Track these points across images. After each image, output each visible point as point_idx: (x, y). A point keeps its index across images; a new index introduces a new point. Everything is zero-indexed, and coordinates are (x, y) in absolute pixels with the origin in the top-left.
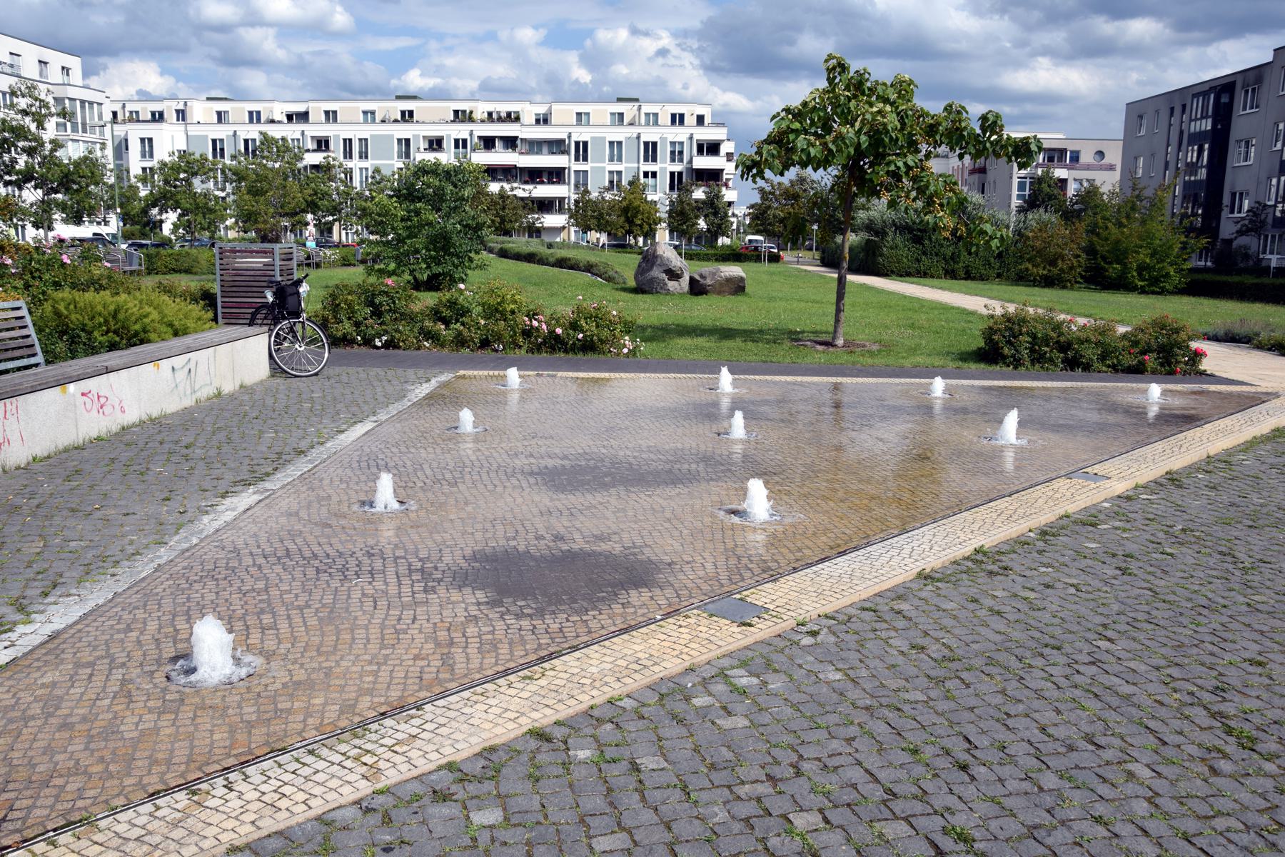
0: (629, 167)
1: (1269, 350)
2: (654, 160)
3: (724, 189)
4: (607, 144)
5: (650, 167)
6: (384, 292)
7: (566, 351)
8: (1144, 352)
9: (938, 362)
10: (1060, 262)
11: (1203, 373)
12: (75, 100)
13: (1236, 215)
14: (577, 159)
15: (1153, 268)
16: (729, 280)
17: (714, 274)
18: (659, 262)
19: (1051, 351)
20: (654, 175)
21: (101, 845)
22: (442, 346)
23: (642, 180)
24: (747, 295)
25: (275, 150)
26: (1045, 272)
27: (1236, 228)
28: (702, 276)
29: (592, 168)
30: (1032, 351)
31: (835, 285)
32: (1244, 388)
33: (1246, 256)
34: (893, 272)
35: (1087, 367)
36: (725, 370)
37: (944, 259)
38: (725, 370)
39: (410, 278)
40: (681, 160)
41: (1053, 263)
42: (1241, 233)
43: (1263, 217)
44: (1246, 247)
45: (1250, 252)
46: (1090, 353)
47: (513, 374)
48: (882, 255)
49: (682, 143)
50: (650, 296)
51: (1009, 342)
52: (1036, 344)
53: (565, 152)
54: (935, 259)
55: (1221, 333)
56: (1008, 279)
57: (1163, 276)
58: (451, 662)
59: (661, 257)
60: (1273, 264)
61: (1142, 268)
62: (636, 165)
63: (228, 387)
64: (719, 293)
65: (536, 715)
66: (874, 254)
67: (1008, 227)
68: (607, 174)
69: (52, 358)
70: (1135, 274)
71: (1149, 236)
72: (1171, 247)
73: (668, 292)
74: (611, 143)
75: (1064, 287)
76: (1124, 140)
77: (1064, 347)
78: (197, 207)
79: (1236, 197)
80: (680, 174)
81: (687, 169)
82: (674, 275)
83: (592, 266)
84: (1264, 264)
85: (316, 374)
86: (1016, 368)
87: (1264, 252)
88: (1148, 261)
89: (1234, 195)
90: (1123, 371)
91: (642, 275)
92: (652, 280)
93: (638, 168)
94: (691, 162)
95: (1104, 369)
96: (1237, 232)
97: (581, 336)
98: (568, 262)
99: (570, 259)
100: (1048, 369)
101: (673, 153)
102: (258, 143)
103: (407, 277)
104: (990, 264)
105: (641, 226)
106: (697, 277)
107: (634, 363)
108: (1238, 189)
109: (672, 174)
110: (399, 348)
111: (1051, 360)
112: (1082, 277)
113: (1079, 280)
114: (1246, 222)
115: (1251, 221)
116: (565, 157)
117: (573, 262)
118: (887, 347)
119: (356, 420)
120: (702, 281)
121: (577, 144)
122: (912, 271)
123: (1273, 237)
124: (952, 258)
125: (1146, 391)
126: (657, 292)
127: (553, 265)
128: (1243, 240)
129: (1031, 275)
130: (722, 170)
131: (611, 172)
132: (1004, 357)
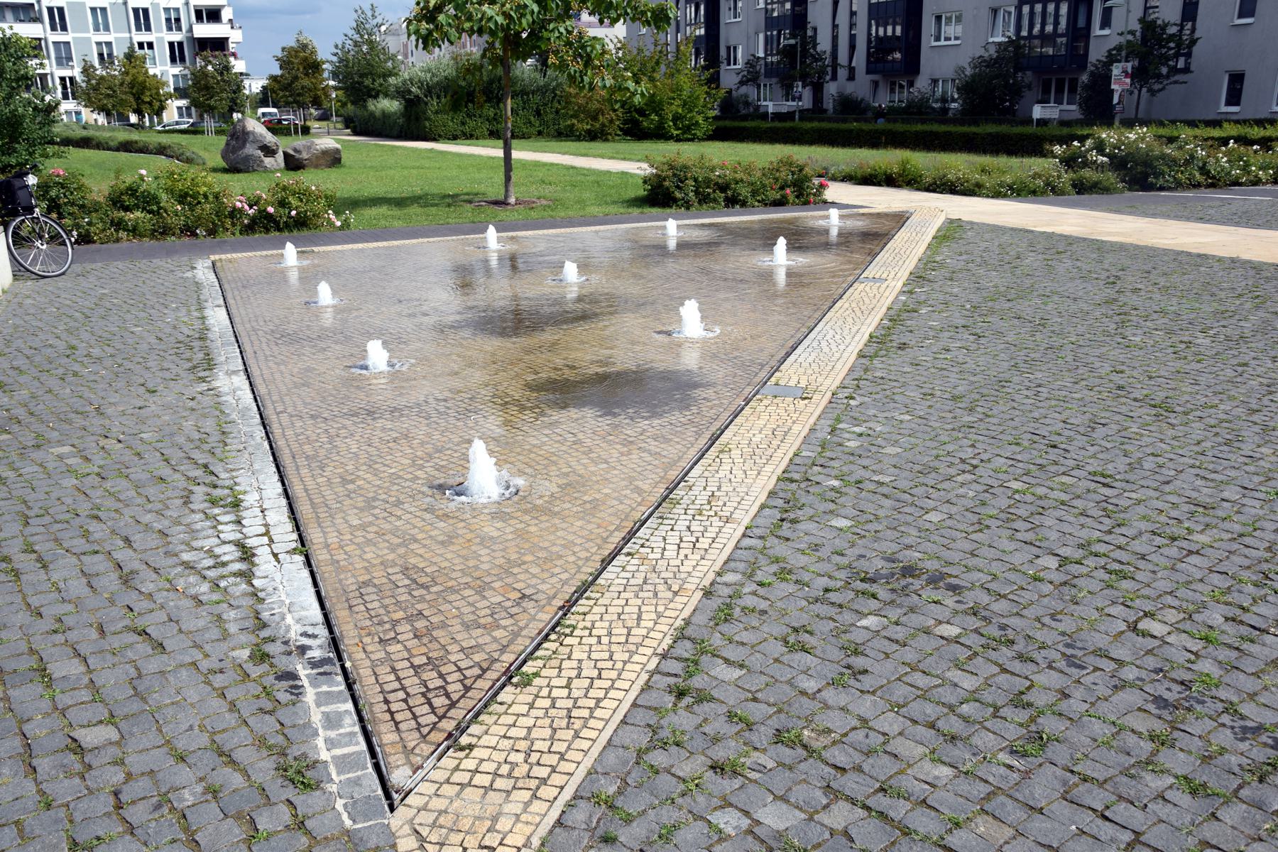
0: (120, 37)
1: (842, 181)
2: (148, 28)
3: (232, 59)
4: (89, 11)
5: (144, 37)
7: (279, 230)
8: (782, 188)
9: (613, 209)
10: (601, 117)
11: (825, 202)
13: (732, 67)
14: (53, 28)
15: (685, 117)
16: (325, 153)
17: (309, 148)
18: (251, 138)
19: (714, 191)
20: (150, 46)
21: (514, 589)
22: (142, 236)
23: (139, 52)
26: (589, 127)
27: (737, 79)
28: (295, 150)
29: (116, 39)
30: (697, 193)
33: (747, 104)
34: (440, 136)
35: (744, 204)
36: (491, 229)
37: (488, 120)
38: (491, 229)
40: (179, 29)
41: (595, 118)
42: (742, 83)
43: (758, 68)
44: (746, 96)
45: (750, 100)
46: (744, 192)
47: (290, 250)
48: (428, 119)
49: (177, 10)
50: (246, 175)
51: (678, 187)
52: (700, 187)
53: (37, 19)
54: (480, 120)
56: (548, 135)
57: (693, 124)
59: (253, 133)
60: (770, 110)
61: (676, 118)
62: (127, 35)
64: (316, 167)
66: (417, 119)
67: (168, 86)
68: (94, 46)
69: (727, 206)
70: (671, 124)
71: (678, 89)
72: (697, 98)
73: (266, 170)
74: (93, 10)
75: (606, 140)
77: (723, 188)
79: (731, 50)
80: (180, 44)
81: (188, 38)
82: (269, 151)
83: (165, 148)
84: (762, 110)
85: (63, 274)
86: (688, 208)
87: (759, 100)
88: (680, 111)
89: (728, 48)
90: (771, 205)
91: (233, 153)
92: (247, 158)
93: (131, 38)
94: (190, 30)
95: (756, 204)
96: (740, 83)
97: (293, 213)
98: (135, 146)
99: (136, 142)
100: (714, 208)
101: (168, 20)
104: (530, 123)
105: (150, 103)
106: (292, 152)
107: (345, 233)
108: (732, 43)
109: (171, 44)
110: (94, 242)
111: (715, 200)
112: (621, 129)
113: (619, 132)
114: (745, 73)
115: (748, 72)
116: (39, 26)
117: (141, 145)
118: (556, 203)
120: (297, 156)
121: (50, 10)
122: (459, 133)
123: (765, 85)
124: (495, 119)
125: (827, 217)
126: (254, 170)
127: (117, 150)
128: (744, 90)
129: (577, 130)
130: (227, 39)
131: (99, 44)
132: (675, 200)
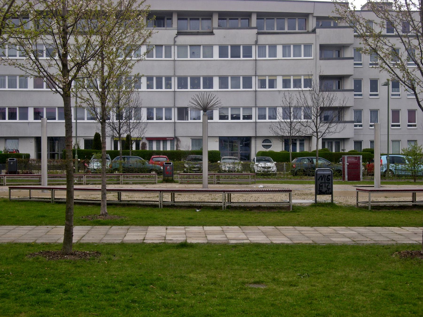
6: (109, 291)
12: (162, 46)
24: (214, 34)
25: (257, 270)
31: (416, 100)
32: (354, 185)
39: (208, 273)
55: (20, 140)
58: (344, 277)
63: (74, 234)
65: (224, 215)
76: (203, 226)
78: (375, 50)
102: (242, 145)
103: (370, 287)
119: (132, 144)
